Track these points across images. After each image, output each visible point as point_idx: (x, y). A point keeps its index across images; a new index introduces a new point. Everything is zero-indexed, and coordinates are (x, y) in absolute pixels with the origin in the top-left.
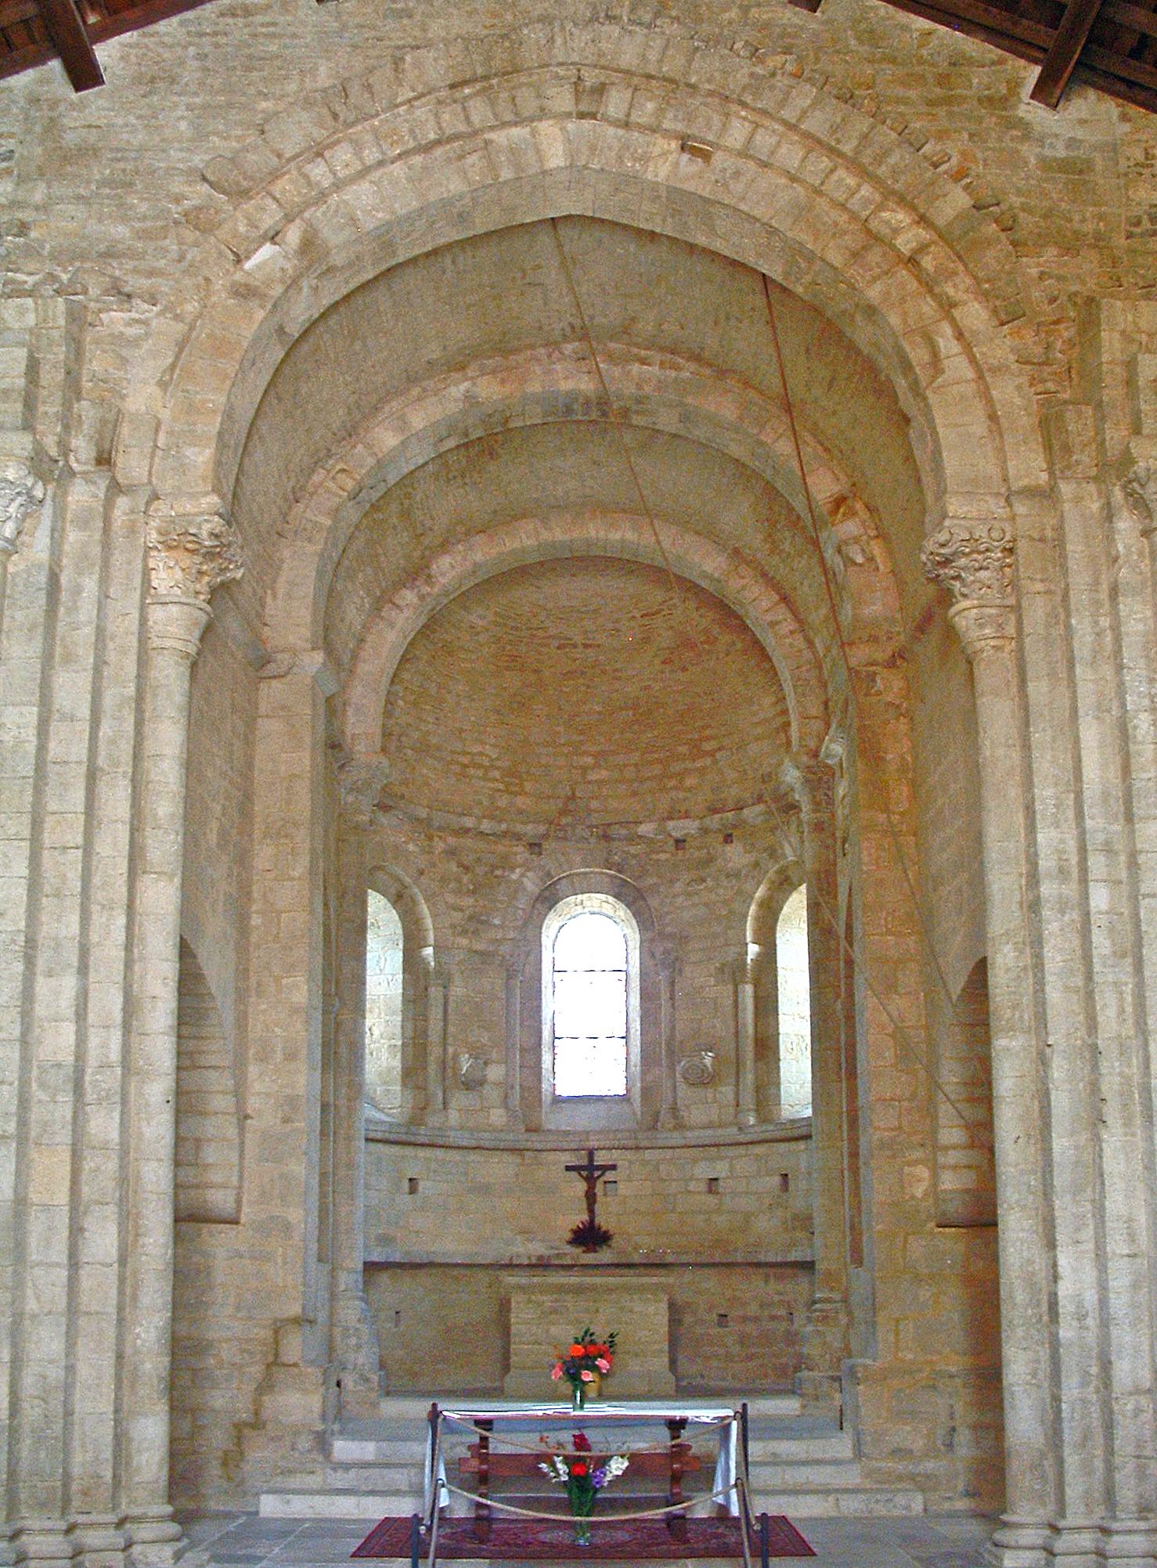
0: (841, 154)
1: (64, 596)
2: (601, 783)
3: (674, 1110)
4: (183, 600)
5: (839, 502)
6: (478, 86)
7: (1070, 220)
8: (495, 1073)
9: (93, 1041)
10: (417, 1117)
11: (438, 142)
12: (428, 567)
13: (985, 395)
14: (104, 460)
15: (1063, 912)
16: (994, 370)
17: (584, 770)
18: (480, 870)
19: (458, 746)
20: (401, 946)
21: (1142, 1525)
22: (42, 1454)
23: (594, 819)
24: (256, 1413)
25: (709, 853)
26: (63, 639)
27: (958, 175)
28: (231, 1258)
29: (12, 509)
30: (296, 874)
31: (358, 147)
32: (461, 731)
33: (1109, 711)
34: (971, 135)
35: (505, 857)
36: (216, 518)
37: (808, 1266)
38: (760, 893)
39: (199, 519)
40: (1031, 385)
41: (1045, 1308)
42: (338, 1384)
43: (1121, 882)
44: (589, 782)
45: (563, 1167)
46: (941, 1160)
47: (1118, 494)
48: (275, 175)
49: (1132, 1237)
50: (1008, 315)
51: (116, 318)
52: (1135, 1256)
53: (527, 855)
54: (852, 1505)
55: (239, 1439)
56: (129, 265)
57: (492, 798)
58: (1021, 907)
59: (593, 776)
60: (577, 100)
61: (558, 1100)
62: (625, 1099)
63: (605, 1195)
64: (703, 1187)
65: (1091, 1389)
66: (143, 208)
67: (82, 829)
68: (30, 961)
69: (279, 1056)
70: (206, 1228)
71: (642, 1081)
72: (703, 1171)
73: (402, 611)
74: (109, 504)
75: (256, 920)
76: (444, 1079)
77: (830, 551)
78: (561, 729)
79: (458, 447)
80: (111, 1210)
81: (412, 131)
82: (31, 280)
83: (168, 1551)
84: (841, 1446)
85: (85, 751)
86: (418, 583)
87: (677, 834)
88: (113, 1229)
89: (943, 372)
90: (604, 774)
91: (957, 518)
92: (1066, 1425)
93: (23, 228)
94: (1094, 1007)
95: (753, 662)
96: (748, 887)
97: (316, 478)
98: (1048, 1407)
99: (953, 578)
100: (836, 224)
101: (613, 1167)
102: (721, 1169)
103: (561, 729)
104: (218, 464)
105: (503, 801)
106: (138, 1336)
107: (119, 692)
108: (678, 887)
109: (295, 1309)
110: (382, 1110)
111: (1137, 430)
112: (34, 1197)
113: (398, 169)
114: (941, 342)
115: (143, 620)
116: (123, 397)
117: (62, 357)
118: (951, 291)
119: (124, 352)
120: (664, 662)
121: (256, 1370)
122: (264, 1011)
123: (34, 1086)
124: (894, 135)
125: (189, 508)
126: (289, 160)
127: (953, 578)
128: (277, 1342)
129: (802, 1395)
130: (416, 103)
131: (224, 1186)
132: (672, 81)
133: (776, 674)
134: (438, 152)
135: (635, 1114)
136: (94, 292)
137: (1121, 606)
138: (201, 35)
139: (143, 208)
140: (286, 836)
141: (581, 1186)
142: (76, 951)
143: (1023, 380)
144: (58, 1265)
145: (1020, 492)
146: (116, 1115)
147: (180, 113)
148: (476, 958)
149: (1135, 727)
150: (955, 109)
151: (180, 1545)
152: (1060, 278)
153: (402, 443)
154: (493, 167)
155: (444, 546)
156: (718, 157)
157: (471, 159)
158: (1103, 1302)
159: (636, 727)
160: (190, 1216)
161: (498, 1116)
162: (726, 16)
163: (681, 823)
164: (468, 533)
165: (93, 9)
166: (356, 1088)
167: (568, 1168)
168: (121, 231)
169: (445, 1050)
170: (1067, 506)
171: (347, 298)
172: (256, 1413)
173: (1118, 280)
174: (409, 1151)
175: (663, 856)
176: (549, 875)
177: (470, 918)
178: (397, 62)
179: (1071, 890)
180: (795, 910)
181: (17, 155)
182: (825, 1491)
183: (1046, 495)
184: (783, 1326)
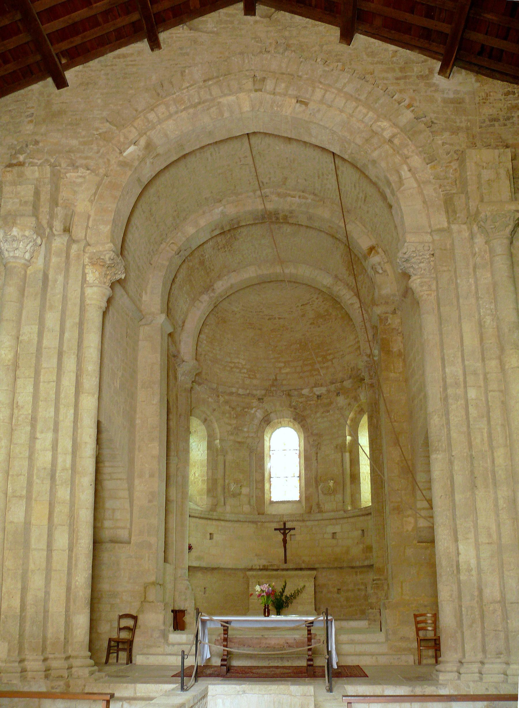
0: (360, 100)
1: (50, 283)
2: (287, 374)
3: (318, 504)
6: (215, 81)
7: (455, 122)
8: (245, 490)
9: (60, 460)
10: (214, 508)
11: (199, 103)
12: (212, 286)
13: (421, 193)
14: (67, 230)
15: (457, 401)
17: (280, 369)
18: (239, 409)
19: (229, 359)
21: (499, 660)
22: (35, 628)
23: (285, 388)
25: (330, 400)
26: (49, 300)
27: (409, 106)
29: (28, 248)
31: (167, 106)
34: (414, 91)
36: (112, 252)
37: (371, 566)
38: (352, 415)
39: (104, 253)
40: (440, 188)
41: (455, 568)
43: (480, 387)
44: (283, 374)
45: (273, 528)
47: (475, 228)
48: (135, 118)
49: (490, 536)
50: (431, 159)
51: (71, 175)
53: (257, 403)
56: (78, 155)
58: (441, 400)
59: (284, 371)
60: (254, 85)
61: (272, 503)
62: (299, 502)
63: (291, 540)
64: (330, 536)
65: (475, 601)
66: (84, 133)
67: (56, 374)
69: (147, 476)
70: (117, 545)
71: (306, 494)
72: (330, 529)
75: (138, 421)
76: (224, 493)
77: (369, 270)
80: (66, 528)
81: (189, 99)
82: (39, 162)
83: (87, 671)
84: (381, 637)
85: (58, 343)
86: (209, 292)
87: (318, 393)
88: (67, 536)
89: (404, 185)
90: (288, 370)
91: (409, 242)
92: (464, 617)
94: (471, 439)
95: (345, 322)
97: (162, 246)
100: (359, 128)
101: (294, 529)
102: (337, 529)
103: (271, 352)
104: (113, 232)
106: (77, 581)
107: (71, 322)
108: (318, 415)
109: (153, 579)
110: (198, 506)
111: (482, 200)
112: (33, 521)
113: (184, 114)
114: (403, 173)
115: (83, 293)
116: (75, 206)
117: (49, 189)
118: (406, 152)
119: (76, 189)
120: (311, 324)
123: (35, 477)
124: (382, 91)
125: (101, 248)
126: (140, 112)
127: (410, 267)
128: (145, 592)
129: (369, 620)
130: (190, 88)
131: (124, 528)
132: (292, 75)
133: (355, 327)
134: (200, 107)
135: (303, 507)
136: (64, 165)
137: (477, 273)
138: (106, 66)
139: (84, 133)
141: (281, 537)
142: (53, 423)
143: (437, 186)
144: (42, 549)
145: (435, 231)
147: (98, 96)
150: (407, 80)
151: (93, 669)
152: (451, 144)
153: (196, 231)
154: (221, 113)
155: (219, 277)
156: (312, 105)
157: (212, 110)
158: (478, 564)
159: (301, 351)
160: (110, 540)
161: (246, 508)
162: (314, 49)
163: (318, 389)
164: (229, 272)
165: (64, 57)
166: (184, 495)
167: (276, 529)
168: (74, 142)
170: (454, 235)
173: (475, 144)
174: (209, 522)
175: (312, 402)
176: (266, 410)
177: (235, 428)
178: (182, 73)
179: (460, 391)
180: (364, 420)
181: (35, 115)
183: (448, 230)
184: (363, 593)
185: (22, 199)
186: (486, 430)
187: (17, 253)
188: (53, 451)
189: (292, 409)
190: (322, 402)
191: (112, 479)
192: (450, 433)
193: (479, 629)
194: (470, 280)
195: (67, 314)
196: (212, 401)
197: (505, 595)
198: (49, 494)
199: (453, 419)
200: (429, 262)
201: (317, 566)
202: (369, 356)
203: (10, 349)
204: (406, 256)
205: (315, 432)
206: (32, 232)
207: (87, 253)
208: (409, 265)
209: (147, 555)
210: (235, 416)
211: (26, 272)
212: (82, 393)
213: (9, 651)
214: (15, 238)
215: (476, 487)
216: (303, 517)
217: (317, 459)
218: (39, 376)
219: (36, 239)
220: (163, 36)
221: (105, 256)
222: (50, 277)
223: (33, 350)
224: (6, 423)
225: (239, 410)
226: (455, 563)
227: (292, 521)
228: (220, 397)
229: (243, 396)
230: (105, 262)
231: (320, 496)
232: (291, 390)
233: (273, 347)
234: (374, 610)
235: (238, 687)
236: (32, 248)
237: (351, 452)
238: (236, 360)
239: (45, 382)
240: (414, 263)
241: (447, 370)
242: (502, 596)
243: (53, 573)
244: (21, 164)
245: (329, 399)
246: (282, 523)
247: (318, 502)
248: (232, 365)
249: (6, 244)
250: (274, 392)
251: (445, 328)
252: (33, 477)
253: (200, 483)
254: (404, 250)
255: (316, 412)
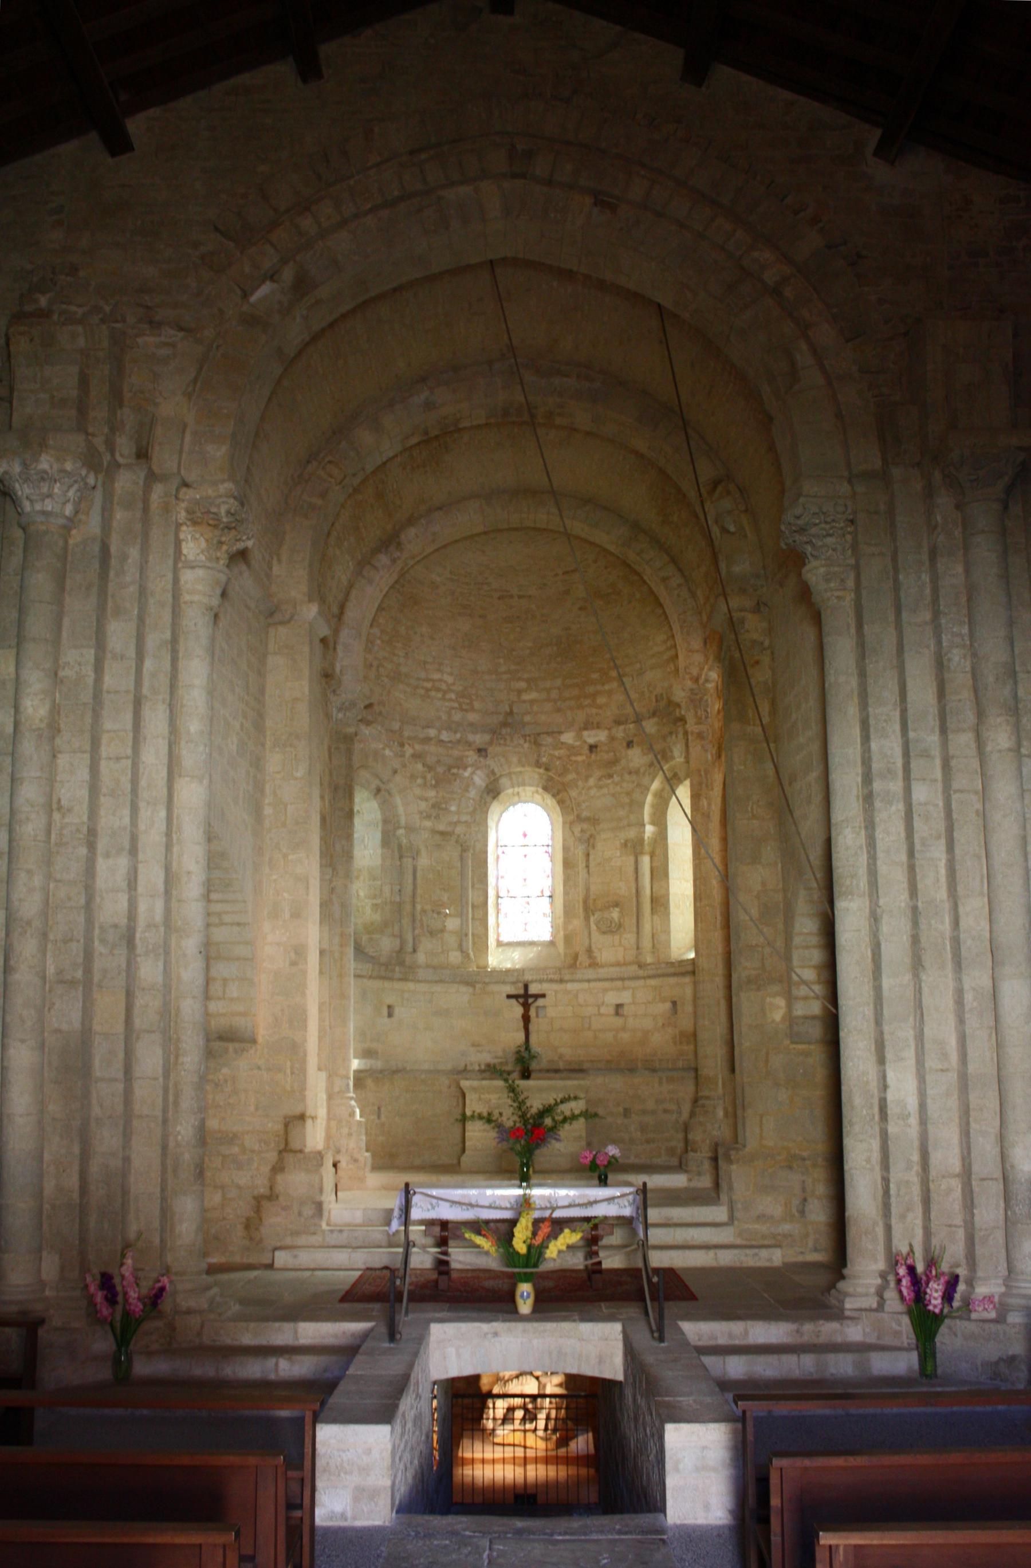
1: (113, 562)
2: (532, 702)
3: (589, 951)
4: (208, 564)
5: (716, 484)
9: (142, 907)
15: (891, 803)
16: (72, 983)
17: (519, 692)
18: (440, 770)
19: (423, 675)
20: (380, 828)
24: (271, 1188)
28: (252, 1069)
29: (71, 493)
30: (299, 775)
32: (425, 663)
33: (928, 647)
35: (461, 758)
36: (232, 501)
39: (218, 501)
41: (876, 1110)
42: (335, 1165)
43: (936, 781)
44: (524, 702)
45: (504, 995)
46: (795, 992)
47: (937, 475)
52: (947, 1070)
54: (726, 1258)
55: (258, 1209)
57: (450, 715)
58: (858, 800)
59: (526, 697)
62: (552, 943)
63: (537, 1016)
65: (913, 1172)
68: (91, 846)
73: (378, 571)
74: (147, 490)
75: (268, 811)
78: (501, 661)
79: (419, 444)
82: (80, 311)
87: (591, 741)
88: (159, 1052)
93: (74, 270)
96: (645, 781)
98: (880, 1186)
99: (807, 543)
101: (543, 996)
102: (625, 997)
103: (501, 661)
105: (457, 717)
108: (592, 782)
112: (97, 1027)
115: (176, 581)
120: (581, 609)
121: (272, 1156)
122: (275, 880)
123: (96, 943)
128: (286, 1133)
137: (939, 565)
140: (291, 745)
141: (519, 1010)
146: (161, 964)
148: (437, 837)
149: (949, 660)
159: (559, 659)
163: (593, 732)
167: (509, 997)
169: (414, 907)
171: (331, 325)
172: (271, 1188)
175: (580, 758)
176: (493, 772)
177: (434, 806)
179: (896, 786)
182: (706, 1247)
185: (55, 394)
186: (944, 861)
187: (49, 505)
188: (129, 892)
189: (542, 771)
190: (598, 758)
191: (222, 924)
192: (875, 864)
193: (919, 1222)
194: (923, 576)
195: (147, 622)
196: (391, 754)
197: (970, 1164)
198: (124, 974)
199: (883, 839)
200: (844, 535)
201: (586, 1066)
202: (696, 680)
203: (42, 696)
204: (800, 522)
205: (585, 814)
206: (79, 464)
207: (183, 501)
208: (805, 539)
209: (289, 1064)
210: (433, 782)
211: (66, 542)
212: (180, 776)
213: (62, 1269)
214: (46, 476)
215: (923, 966)
216: (560, 974)
217: (587, 867)
218: (99, 747)
219: (86, 476)
220: (326, 50)
221: (218, 506)
222: (113, 549)
223: (87, 696)
224: (39, 841)
225: (442, 772)
226: (876, 1102)
227: (541, 981)
228: (407, 746)
229: (450, 745)
230: (218, 520)
231: (593, 936)
232: (539, 734)
233: (506, 651)
234: (699, 1154)
235: (485, 1327)
236: (79, 494)
237: (652, 855)
238: (437, 676)
239: (110, 759)
240: (813, 536)
241: (874, 746)
242: (963, 1165)
243: (136, 1123)
244: (44, 314)
245: (612, 754)
246: (521, 985)
247: (590, 947)
248: (429, 685)
249: (25, 486)
250: (508, 737)
251: (871, 666)
252: (93, 943)
253: (368, 910)
254: (798, 511)
255: (587, 778)
